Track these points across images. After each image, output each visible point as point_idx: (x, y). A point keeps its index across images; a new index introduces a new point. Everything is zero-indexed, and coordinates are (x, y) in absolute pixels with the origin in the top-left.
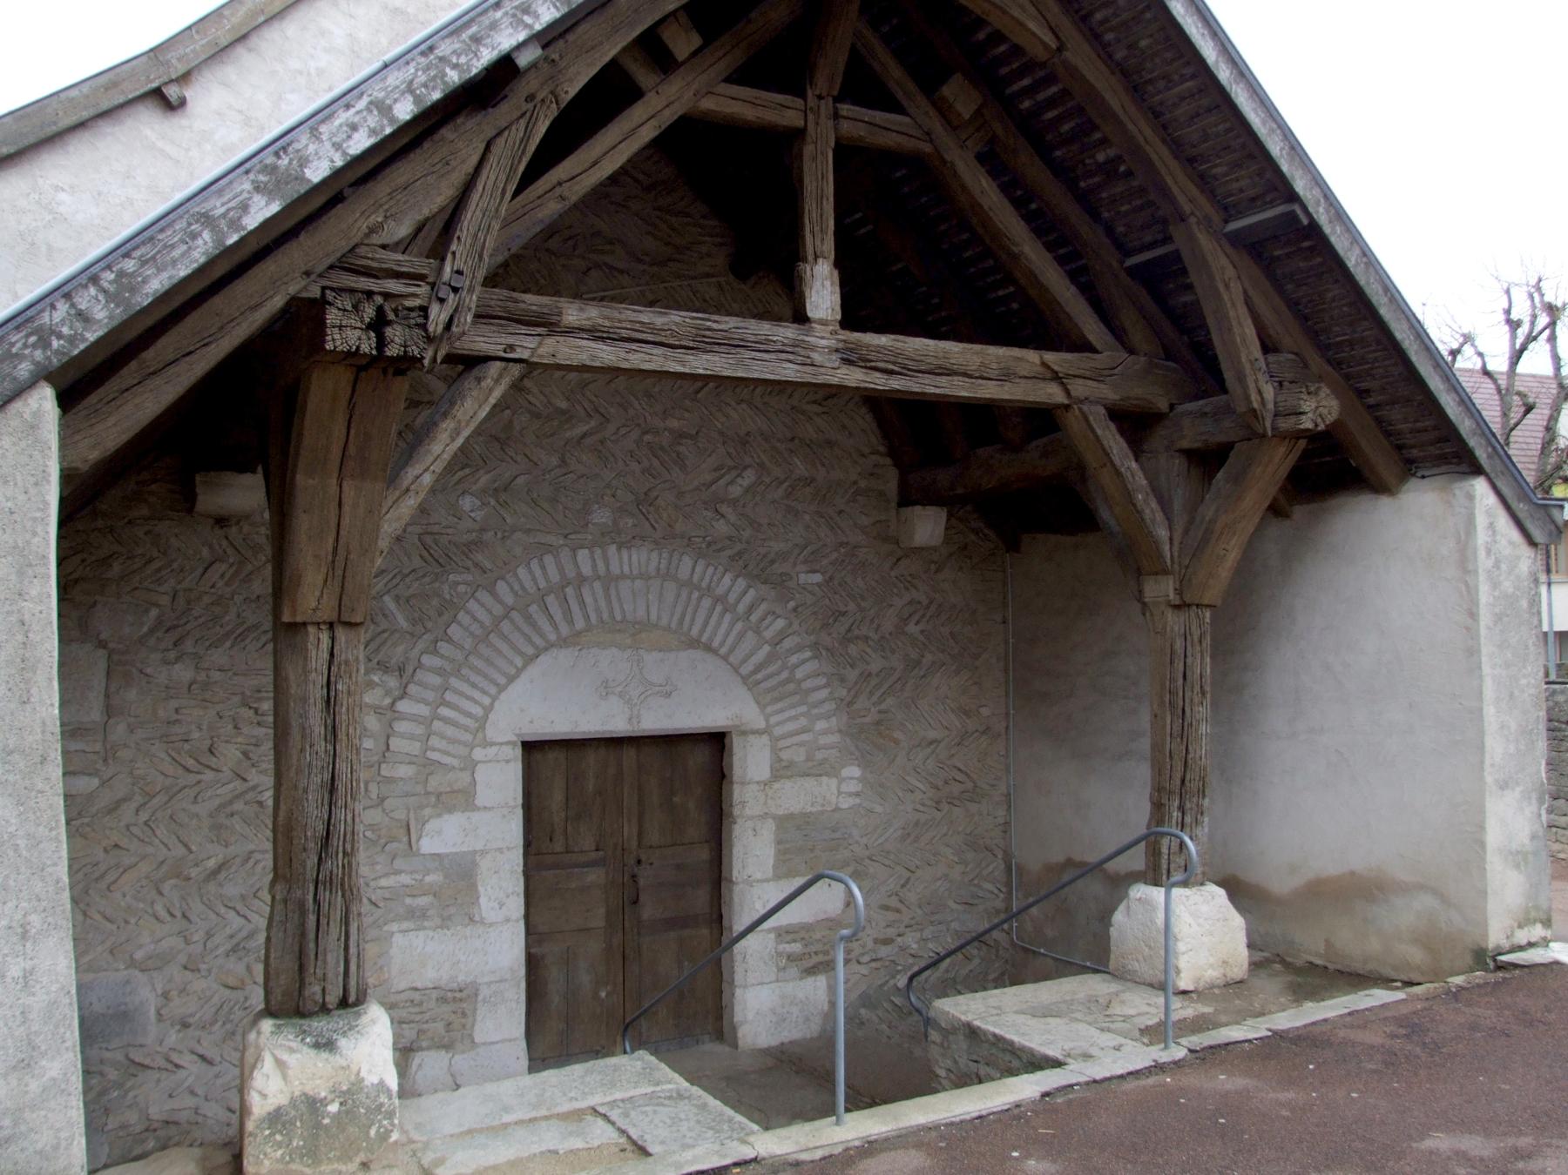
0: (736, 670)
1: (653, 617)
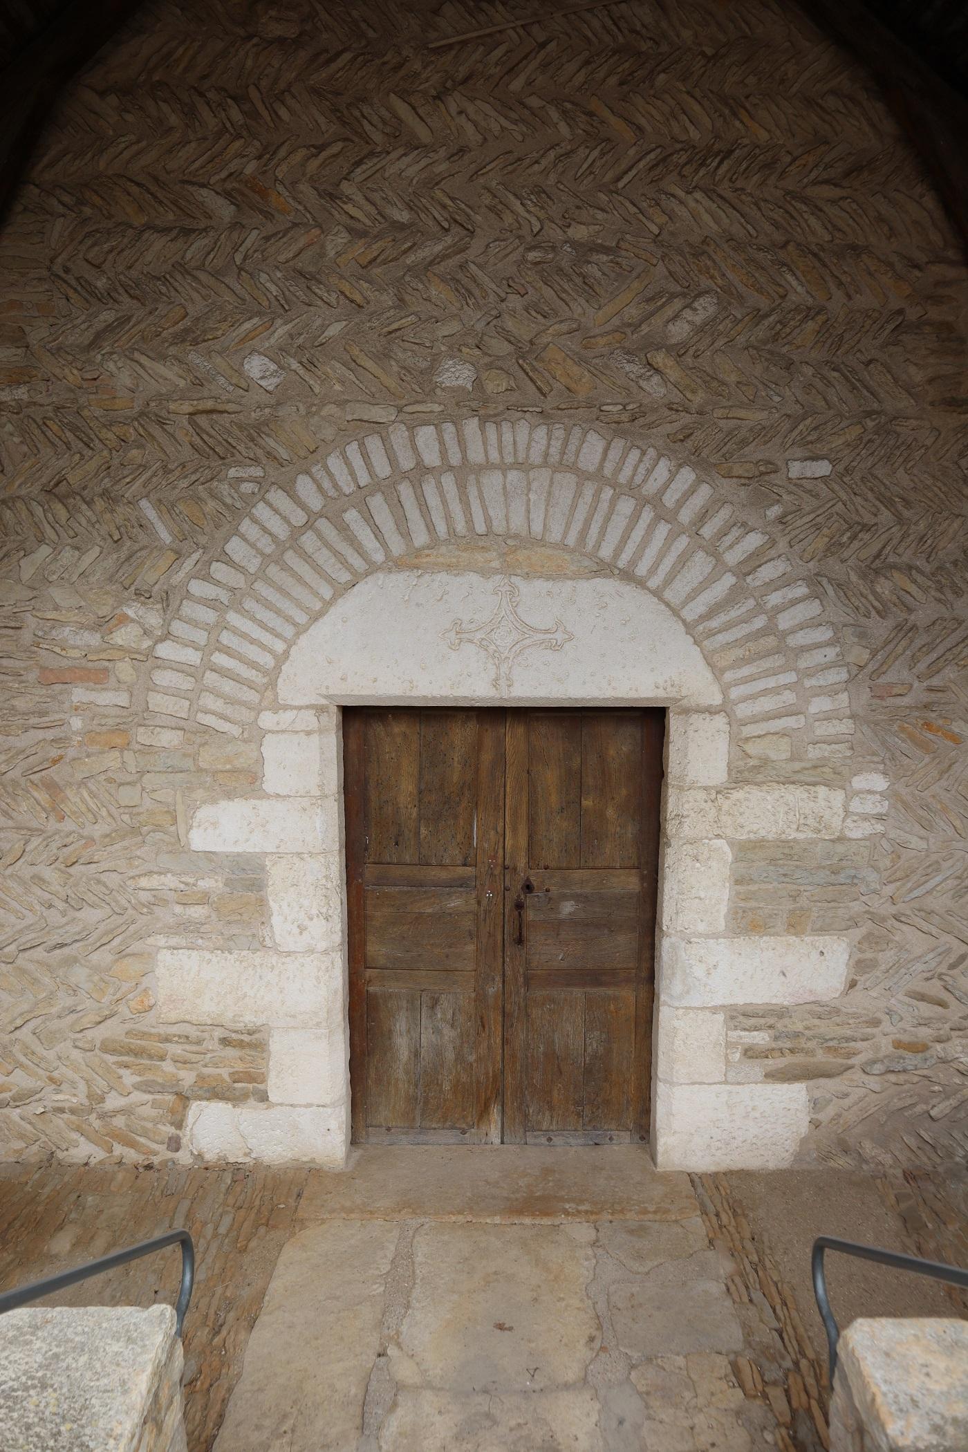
0: (675, 613)
1: (537, 528)
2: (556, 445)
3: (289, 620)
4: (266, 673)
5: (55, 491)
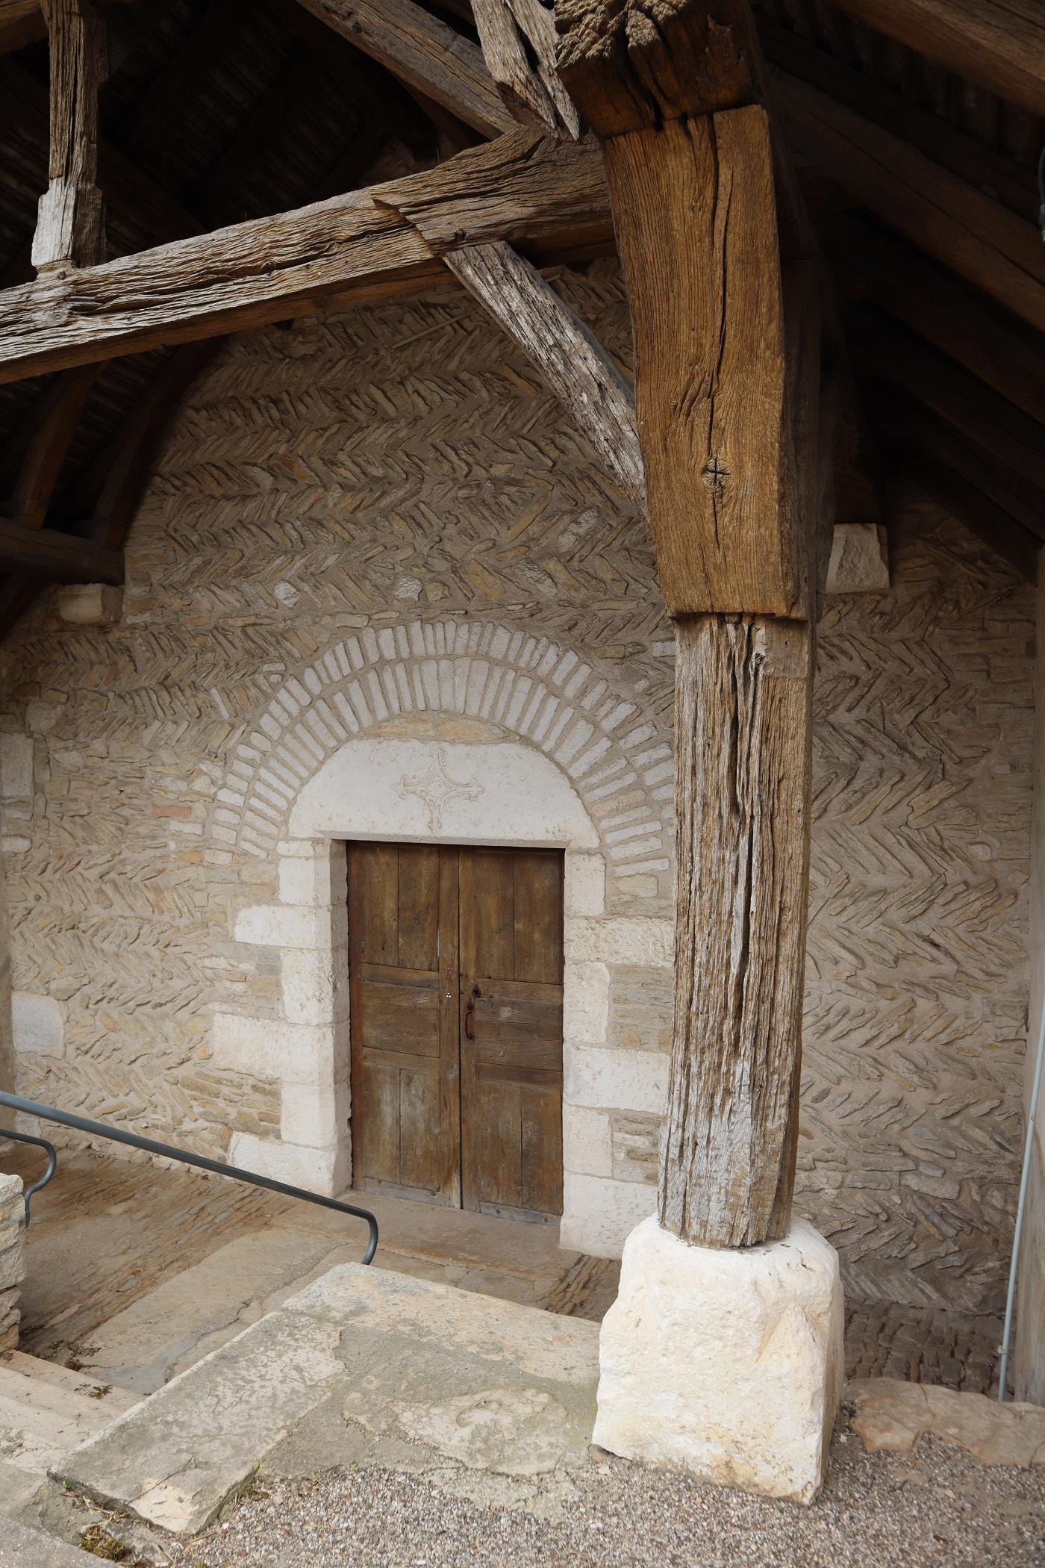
2: (475, 638)
3: (296, 774)
4: (282, 813)
5: (165, 684)
